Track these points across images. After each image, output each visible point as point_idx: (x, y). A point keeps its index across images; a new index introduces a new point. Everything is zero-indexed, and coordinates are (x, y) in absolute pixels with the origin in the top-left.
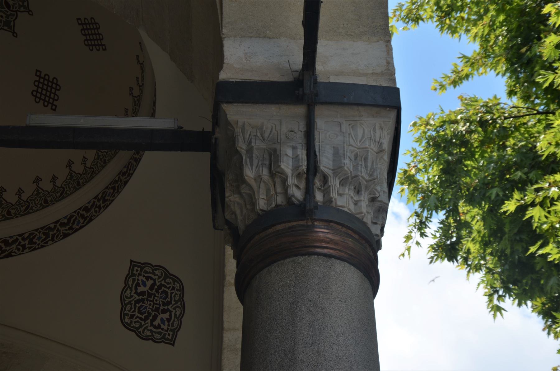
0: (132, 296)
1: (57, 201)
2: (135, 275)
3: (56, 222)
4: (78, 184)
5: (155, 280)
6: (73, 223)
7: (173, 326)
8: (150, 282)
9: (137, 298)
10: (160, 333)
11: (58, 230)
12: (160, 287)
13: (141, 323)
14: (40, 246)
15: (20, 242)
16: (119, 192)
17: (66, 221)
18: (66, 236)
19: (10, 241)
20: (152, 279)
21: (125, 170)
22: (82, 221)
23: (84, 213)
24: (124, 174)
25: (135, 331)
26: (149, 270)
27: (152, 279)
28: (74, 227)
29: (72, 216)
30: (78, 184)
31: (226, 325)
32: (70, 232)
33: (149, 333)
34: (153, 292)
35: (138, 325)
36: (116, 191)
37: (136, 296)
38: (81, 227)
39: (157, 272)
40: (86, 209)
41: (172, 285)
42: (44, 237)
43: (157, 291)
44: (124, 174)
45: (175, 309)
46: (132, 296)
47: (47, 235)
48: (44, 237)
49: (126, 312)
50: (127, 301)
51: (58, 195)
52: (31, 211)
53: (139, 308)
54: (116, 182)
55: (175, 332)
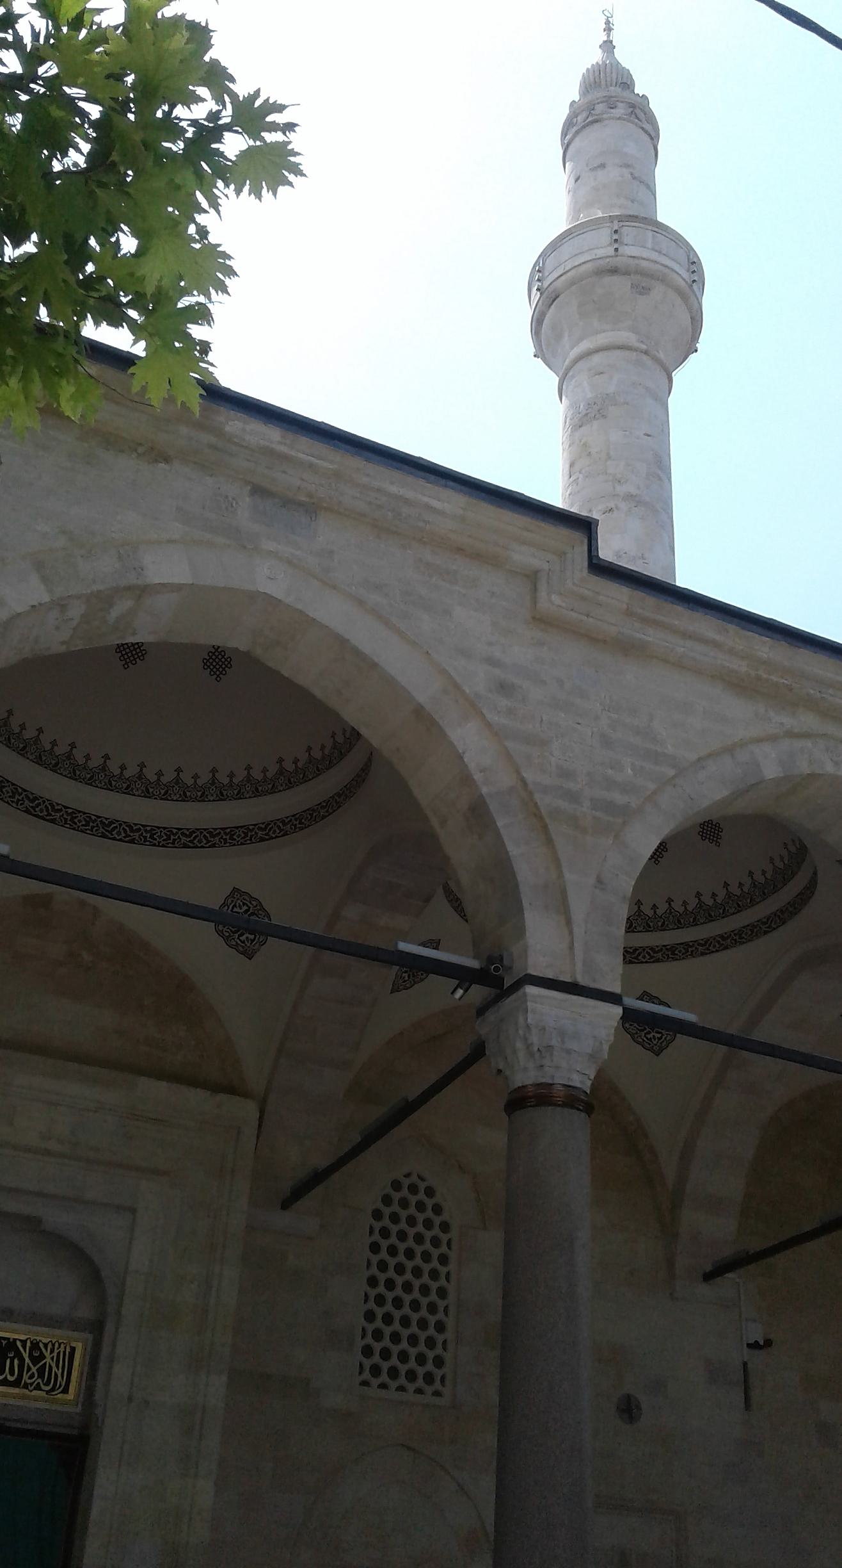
7: (232, 901)
13: (258, 912)
14: (239, 843)
15: (222, 836)
17: (263, 826)
22: (718, 946)
23: (281, 825)
28: (711, 948)
35: (260, 912)
36: (754, 934)
42: (243, 835)
47: (246, 834)
48: (243, 835)
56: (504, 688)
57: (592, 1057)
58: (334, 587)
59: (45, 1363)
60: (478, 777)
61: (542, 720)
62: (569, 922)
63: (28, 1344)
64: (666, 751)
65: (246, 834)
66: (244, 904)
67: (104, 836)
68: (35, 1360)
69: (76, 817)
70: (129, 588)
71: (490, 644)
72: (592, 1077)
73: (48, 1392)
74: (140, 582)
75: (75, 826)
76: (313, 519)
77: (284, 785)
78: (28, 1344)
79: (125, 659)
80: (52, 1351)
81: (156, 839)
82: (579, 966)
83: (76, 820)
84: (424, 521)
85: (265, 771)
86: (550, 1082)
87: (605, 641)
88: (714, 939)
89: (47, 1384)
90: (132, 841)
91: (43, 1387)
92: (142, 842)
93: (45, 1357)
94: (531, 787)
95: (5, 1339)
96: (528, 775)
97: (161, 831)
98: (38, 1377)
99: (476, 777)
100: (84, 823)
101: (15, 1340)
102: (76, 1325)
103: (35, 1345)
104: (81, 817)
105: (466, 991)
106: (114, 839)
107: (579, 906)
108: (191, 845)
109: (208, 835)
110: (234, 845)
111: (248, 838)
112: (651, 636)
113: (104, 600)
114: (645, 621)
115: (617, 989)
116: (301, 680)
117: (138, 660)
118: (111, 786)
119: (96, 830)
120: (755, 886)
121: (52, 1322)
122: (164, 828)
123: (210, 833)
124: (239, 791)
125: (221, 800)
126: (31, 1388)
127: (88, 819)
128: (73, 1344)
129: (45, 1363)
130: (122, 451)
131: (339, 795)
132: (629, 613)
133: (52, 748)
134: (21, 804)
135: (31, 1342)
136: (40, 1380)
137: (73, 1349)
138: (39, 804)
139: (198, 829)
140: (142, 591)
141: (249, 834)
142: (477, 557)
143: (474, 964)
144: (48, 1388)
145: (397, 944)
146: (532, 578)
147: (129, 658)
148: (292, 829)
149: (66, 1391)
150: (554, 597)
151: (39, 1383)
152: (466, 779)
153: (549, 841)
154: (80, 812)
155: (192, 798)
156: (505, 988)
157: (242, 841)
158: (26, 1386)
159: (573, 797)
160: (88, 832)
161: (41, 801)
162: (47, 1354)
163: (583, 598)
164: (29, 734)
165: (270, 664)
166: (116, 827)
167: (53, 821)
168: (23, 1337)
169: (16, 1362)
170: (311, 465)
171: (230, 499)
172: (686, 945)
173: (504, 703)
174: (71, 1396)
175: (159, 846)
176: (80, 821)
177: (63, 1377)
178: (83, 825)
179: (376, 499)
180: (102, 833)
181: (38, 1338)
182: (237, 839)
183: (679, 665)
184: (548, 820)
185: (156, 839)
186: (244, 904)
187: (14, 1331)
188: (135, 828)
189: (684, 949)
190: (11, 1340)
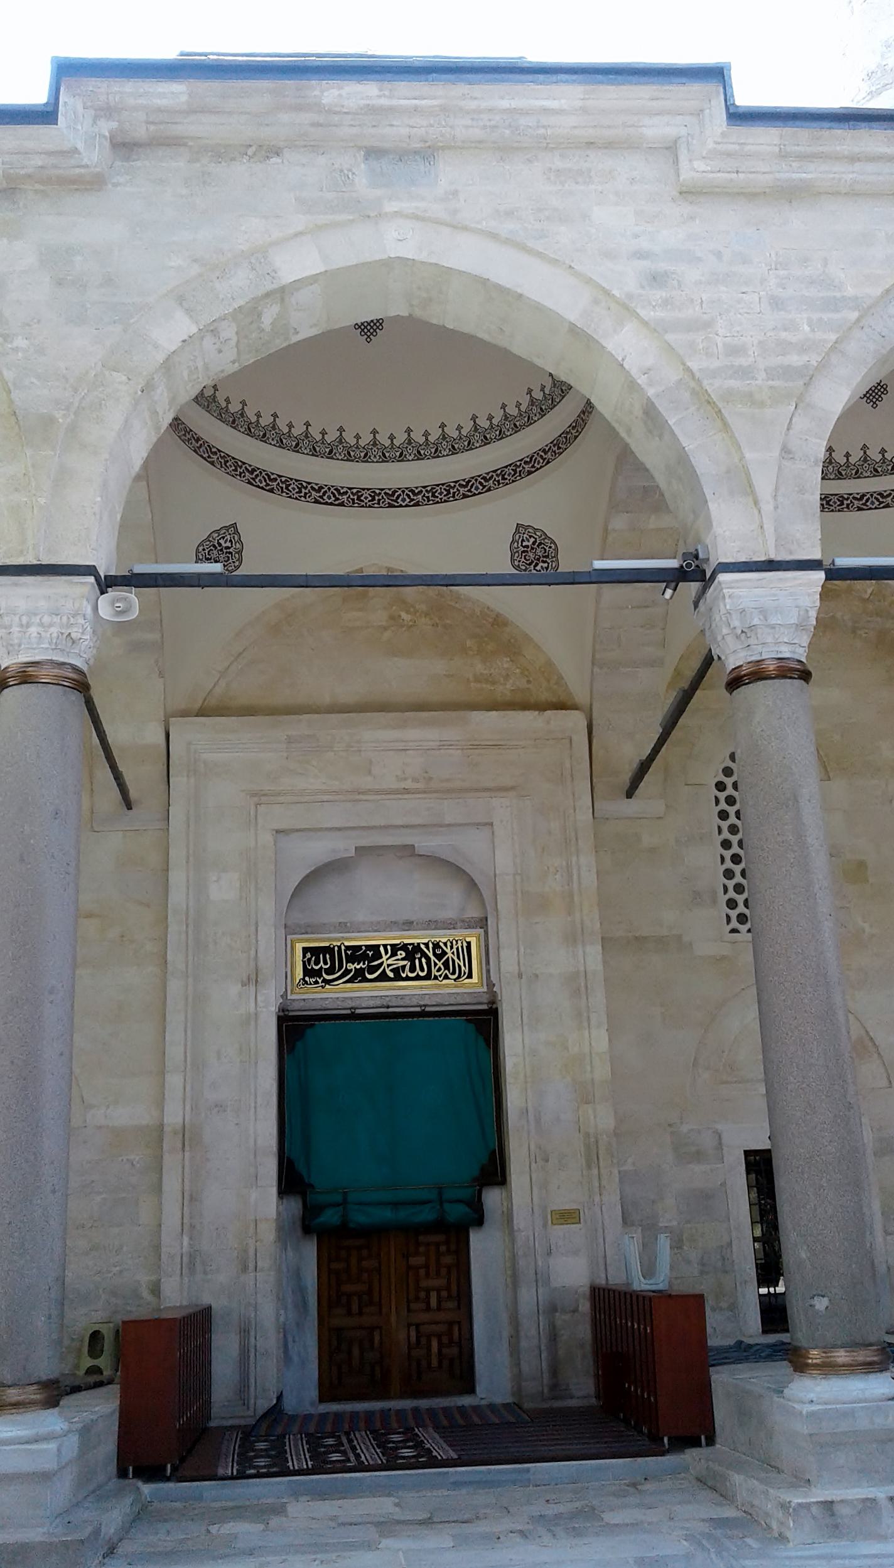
17: (528, 460)
20: (232, 544)
23: (543, 454)
26: (236, 538)
27: (232, 544)
39: (537, 533)
43: (532, 562)
47: (515, 471)
48: (445, 493)
50: (211, 539)
52: (369, 460)
56: (656, 279)
57: (800, 627)
58: (465, 228)
59: (448, 958)
60: (642, 380)
61: (702, 301)
62: (756, 503)
63: (431, 945)
64: (845, 294)
65: (515, 471)
66: (530, 537)
67: (391, 506)
68: (439, 957)
69: (362, 495)
70: (267, 295)
71: (636, 236)
72: (806, 644)
73: (455, 980)
74: (275, 286)
75: (363, 504)
76: (432, 163)
77: (538, 415)
78: (431, 945)
79: (366, 334)
80: (452, 947)
81: (437, 497)
82: (771, 543)
83: (362, 498)
84: (544, 127)
85: (518, 405)
86: (759, 658)
87: (765, 192)
89: (453, 973)
90: (417, 504)
91: (450, 976)
92: (426, 502)
93: (446, 953)
94: (697, 375)
95: (410, 944)
96: (694, 365)
97: (441, 488)
98: (445, 970)
99: (639, 381)
100: (370, 498)
101: (419, 944)
102: (469, 925)
103: (436, 946)
104: (366, 494)
105: (675, 590)
106: (401, 506)
107: (764, 486)
108: (470, 494)
109: (482, 481)
110: (507, 484)
111: (518, 474)
112: (812, 173)
113: (251, 312)
114: (802, 157)
115: (816, 555)
116: (468, 328)
117: (371, 336)
118: (386, 458)
119: (383, 502)
121: (450, 925)
122: (443, 484)
123: (484, 478)
124: (500, 432)
125: (486, 444)
126: (440, 979)
127: (373, 494)
128: (468, 939)
129: (448, 958)
130: (233, 159)
131: (583, 412)
132: (783, 156)
133: (323, 437)
134: (309, 497)
135: (433, 943)
136: (446, 971)
137: (469, 943)
138: (257, 476)
139: (473, 478)
140: (282, 293)
141: (518, 470)
142: (609, 146)
143: (673, 563)
144: (454, 977)
145: (592, 563)
146: (671, 148)
147: (369, 331)
148: (552, 455)
149: (470, 976)
150: (696, 164)
151: (446, 974)
152: (632, 385)
153: (726, 426)
154: (364, 489)
155: (460, 449)
156: (708, 577)
157: (513, 478)
158: (436, 978)
159: (745, 373)
160: (376, 505)
162: (448, 950)
163: (729, 155)
164: (298, 431)
165: (434, 321)
166: (400, 495)
167: (342, 504)
168: (426, 941)
169: (424, 960)
170: (416, 109)
171: (346, 172)
173: (658, 294)
174: (475, 979)
175: (441, 502)
176: (366, 498)
177: (465, 965)
178: (369, 501)
179: (490, 120)
180: (389, 503)
181: (438, 940)
182: (509, 478)
183: (853, 193)
184: (720, 405)
185: (437, 497)
186: (530, 537)
187: (415, 937)
188: (416, 491)
190: (416, 945)
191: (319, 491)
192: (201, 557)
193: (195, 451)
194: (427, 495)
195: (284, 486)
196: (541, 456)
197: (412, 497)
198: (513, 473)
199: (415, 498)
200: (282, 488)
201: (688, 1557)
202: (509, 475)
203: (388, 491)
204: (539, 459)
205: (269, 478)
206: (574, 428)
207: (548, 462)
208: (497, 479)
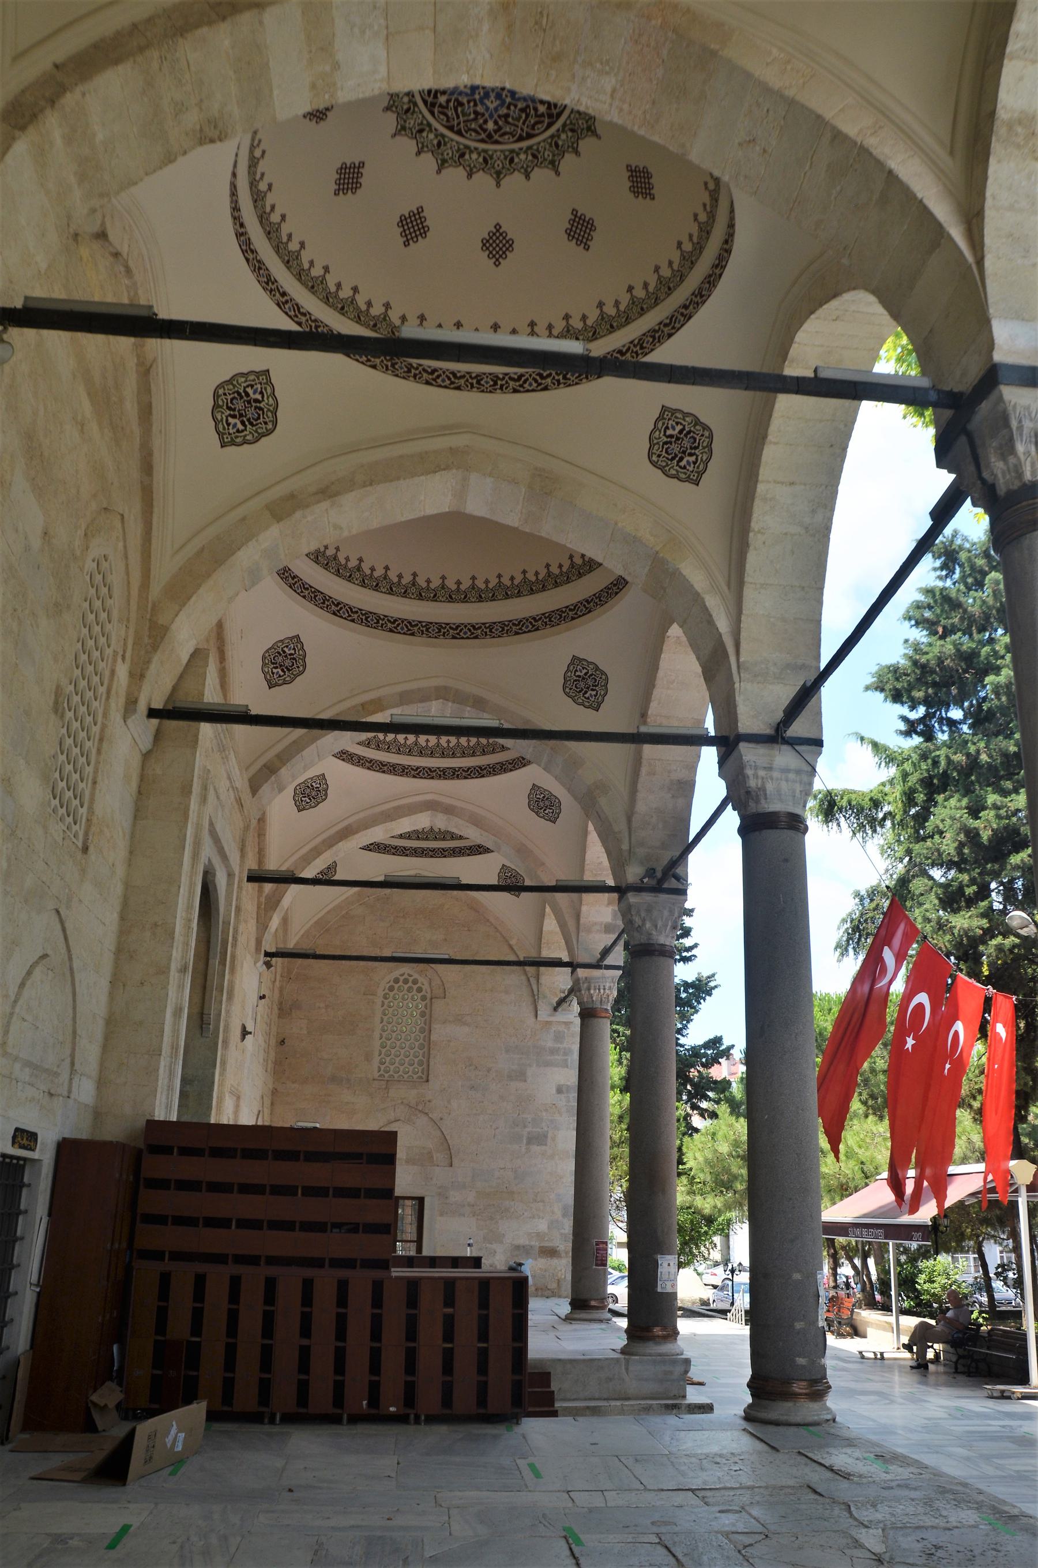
0: (660, 438)
1: (624, 326)
2: (258, 379)
3: (660, 323)
4: (669, 289)
5: (684, 426)
6: (675, 323)
8: (679, 427)
9: (665, 439)
10: (224, 428)
11: (663, 331)
12: (689, 432)
16: (715, 286)
18: (670, 336)
19: (624, 350)
21: (717, 262)
22: (682, 319)
23: (683, 310)
24: (717, 266)
25: (662, 469)
27: (227, 420)
29: (673, 316)
30: (669, 289)
31: (760, 478)
32: (673, 331)
33: (674, 472)
34: (237, 413)
37: (664, 437)
38: (682, 326)
40: (686, 307)
41: (223, 397)
44: (717, 266)
45: (702, 453)
46: (660, 438)
49: (654, 451)
51: (624, 320)
53: (666, 449)
54: (710, 276)
55: (701, 474)
75: (482, 388)
88: (527, 620)
108: (522, 389)
120: (416, 744)
138: (341, 608)
141: (657, 335)
161: (342, 605)
172: (502, 764)
189: (492, 380)
191: (394, 623)
192: (270, 414)
193: (291, 587)
194: (557, 378)
195: (364, 617)
196: (584, 606)
197: (540, 381)
198: (651, 340)
199: (543, 382)
200: (362, 619)
201: (6, 996)
202: (555, 618)
203: (452, 626)
204: (679, 317)
205: (351, 610)
206: (615, 585)
207: (590, 611)
208: (635, 350)
